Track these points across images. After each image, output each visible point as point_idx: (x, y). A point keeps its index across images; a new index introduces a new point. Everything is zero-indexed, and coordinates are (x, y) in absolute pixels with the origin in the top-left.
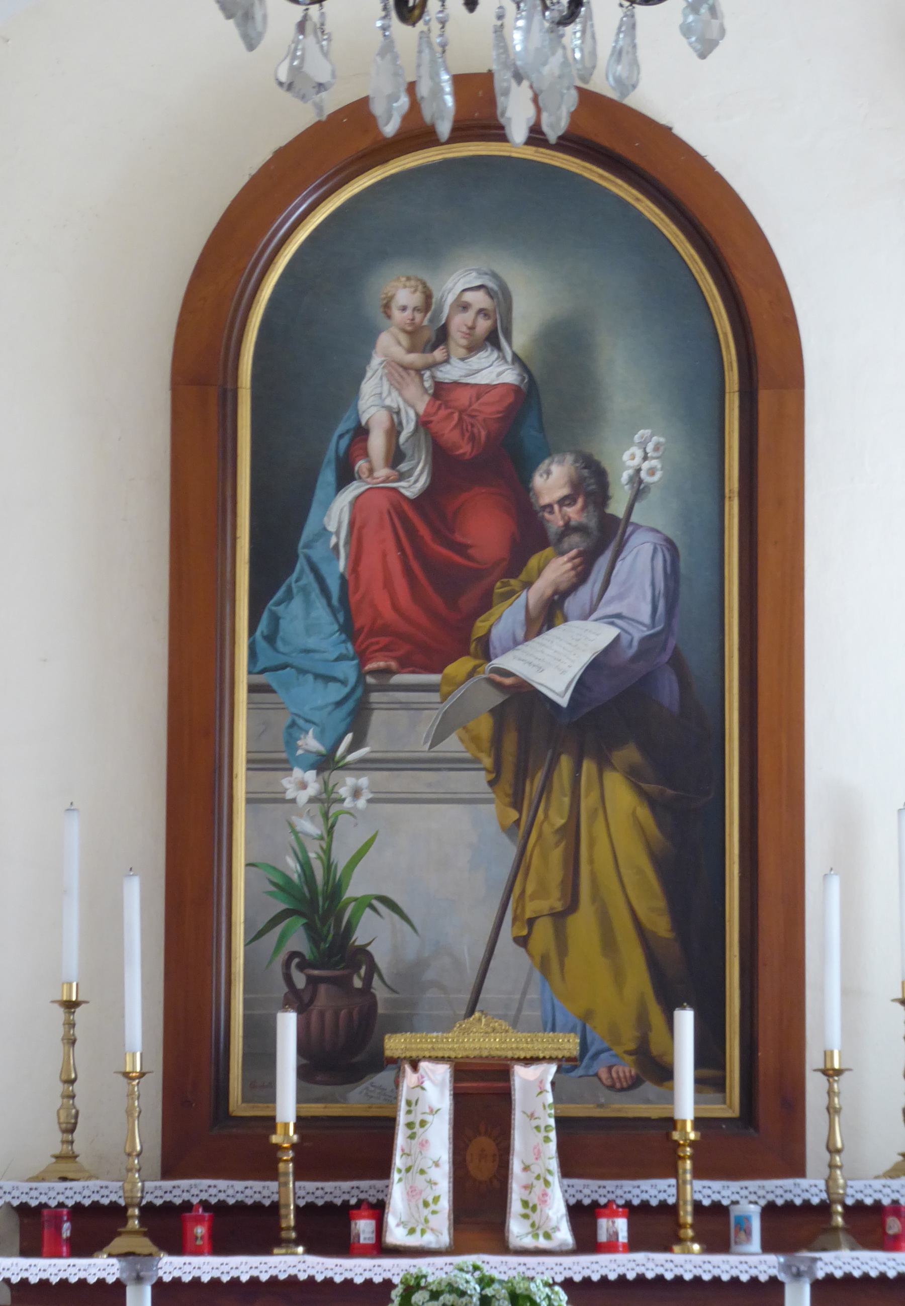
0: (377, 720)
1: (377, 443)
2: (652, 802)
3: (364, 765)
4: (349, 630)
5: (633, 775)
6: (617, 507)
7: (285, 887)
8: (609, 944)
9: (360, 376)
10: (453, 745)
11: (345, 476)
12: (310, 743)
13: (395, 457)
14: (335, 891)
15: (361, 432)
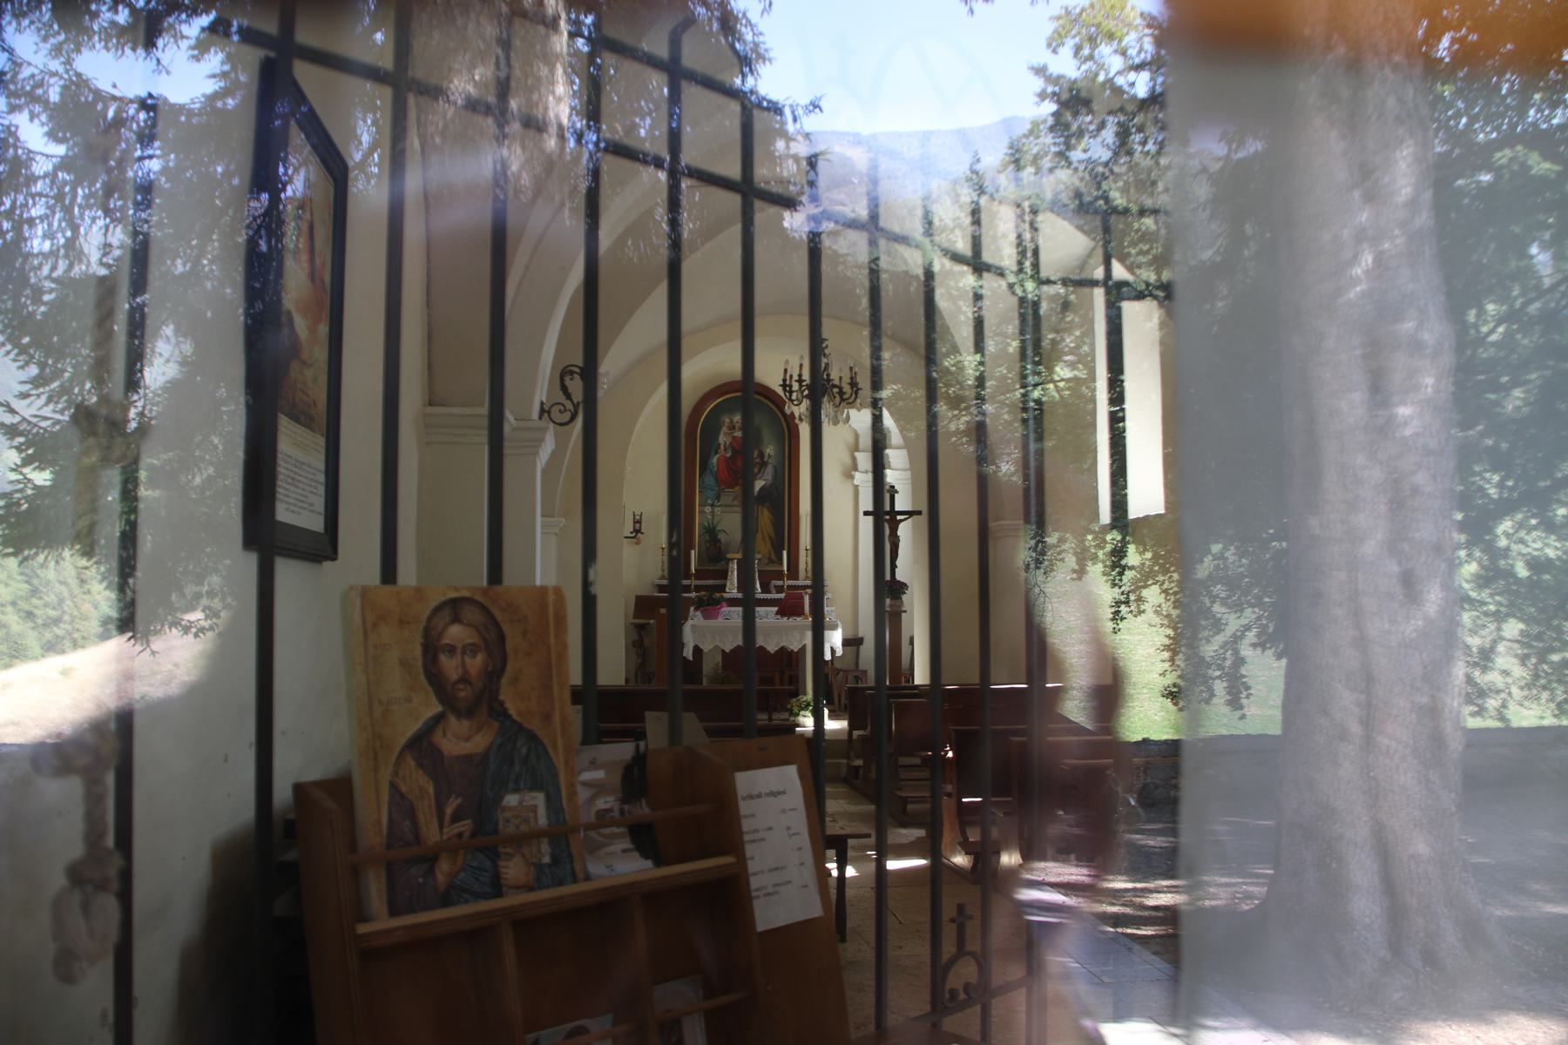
0: (722, 498)
1: (722, 447)
2: (771, 513)
3: (721, 506)
4: (717, 480)
5: (768, 508)
6: (766, 459)
7: (705, 528)
8: (764, 539)
9: (718, 435)
10: (736, 502)
11: (716, 453)
12: (710, 502)
13: (725, 450)
14: (714, 529)
15: (719, 445)
